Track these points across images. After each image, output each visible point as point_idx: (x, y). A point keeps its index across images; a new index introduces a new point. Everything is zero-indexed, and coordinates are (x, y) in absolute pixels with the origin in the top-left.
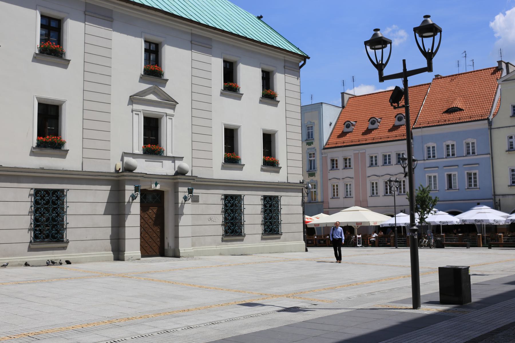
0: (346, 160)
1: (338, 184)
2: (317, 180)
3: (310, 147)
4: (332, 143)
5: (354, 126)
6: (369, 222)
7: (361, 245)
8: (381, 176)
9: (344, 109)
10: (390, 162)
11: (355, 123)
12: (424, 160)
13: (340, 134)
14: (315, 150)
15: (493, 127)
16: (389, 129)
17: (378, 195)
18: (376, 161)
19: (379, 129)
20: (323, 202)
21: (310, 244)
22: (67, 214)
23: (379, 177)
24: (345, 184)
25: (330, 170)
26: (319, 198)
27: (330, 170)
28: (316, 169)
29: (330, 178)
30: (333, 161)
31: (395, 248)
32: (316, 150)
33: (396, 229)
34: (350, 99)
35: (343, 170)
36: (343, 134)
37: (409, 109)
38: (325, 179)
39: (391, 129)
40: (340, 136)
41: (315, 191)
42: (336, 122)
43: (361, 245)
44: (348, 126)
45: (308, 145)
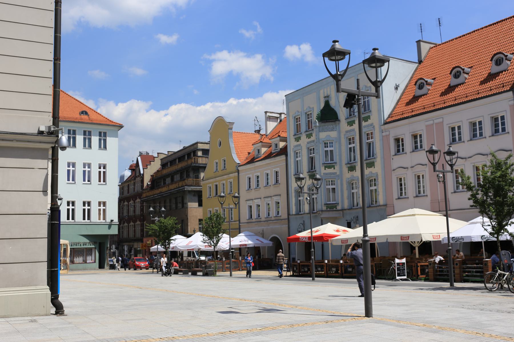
0: (415, 137)
2: (377, 173)
4: (398, 114)
5: (431, 85)
6: (420, 234)
7: (405, 277)
8: (469, 158)
9: (420, 64)
10: (504, 130)
11: (433, 81)
13: (410, 100)
14: (373, 127)
16: (482, 81)
18: (460, 134)
19: (466, 83)
20: (386, 205)
23: (486, 156)
24: (415, 175)
25: (393, 156)
26: (381, 200)
27: (393, 156)
28: (375, 156)
29: (394, 168)
30: (397, 140)
32: (374, 127)
33: (231, 253)
34: (431, 50)
35: (412, 153)
36: (415, 99)
38: (388, 170)
39: (484, 80)
40: (409, 103)
41: (376, 190)
42: (408, 83)
43: (405, 277)
44: (422, 86)
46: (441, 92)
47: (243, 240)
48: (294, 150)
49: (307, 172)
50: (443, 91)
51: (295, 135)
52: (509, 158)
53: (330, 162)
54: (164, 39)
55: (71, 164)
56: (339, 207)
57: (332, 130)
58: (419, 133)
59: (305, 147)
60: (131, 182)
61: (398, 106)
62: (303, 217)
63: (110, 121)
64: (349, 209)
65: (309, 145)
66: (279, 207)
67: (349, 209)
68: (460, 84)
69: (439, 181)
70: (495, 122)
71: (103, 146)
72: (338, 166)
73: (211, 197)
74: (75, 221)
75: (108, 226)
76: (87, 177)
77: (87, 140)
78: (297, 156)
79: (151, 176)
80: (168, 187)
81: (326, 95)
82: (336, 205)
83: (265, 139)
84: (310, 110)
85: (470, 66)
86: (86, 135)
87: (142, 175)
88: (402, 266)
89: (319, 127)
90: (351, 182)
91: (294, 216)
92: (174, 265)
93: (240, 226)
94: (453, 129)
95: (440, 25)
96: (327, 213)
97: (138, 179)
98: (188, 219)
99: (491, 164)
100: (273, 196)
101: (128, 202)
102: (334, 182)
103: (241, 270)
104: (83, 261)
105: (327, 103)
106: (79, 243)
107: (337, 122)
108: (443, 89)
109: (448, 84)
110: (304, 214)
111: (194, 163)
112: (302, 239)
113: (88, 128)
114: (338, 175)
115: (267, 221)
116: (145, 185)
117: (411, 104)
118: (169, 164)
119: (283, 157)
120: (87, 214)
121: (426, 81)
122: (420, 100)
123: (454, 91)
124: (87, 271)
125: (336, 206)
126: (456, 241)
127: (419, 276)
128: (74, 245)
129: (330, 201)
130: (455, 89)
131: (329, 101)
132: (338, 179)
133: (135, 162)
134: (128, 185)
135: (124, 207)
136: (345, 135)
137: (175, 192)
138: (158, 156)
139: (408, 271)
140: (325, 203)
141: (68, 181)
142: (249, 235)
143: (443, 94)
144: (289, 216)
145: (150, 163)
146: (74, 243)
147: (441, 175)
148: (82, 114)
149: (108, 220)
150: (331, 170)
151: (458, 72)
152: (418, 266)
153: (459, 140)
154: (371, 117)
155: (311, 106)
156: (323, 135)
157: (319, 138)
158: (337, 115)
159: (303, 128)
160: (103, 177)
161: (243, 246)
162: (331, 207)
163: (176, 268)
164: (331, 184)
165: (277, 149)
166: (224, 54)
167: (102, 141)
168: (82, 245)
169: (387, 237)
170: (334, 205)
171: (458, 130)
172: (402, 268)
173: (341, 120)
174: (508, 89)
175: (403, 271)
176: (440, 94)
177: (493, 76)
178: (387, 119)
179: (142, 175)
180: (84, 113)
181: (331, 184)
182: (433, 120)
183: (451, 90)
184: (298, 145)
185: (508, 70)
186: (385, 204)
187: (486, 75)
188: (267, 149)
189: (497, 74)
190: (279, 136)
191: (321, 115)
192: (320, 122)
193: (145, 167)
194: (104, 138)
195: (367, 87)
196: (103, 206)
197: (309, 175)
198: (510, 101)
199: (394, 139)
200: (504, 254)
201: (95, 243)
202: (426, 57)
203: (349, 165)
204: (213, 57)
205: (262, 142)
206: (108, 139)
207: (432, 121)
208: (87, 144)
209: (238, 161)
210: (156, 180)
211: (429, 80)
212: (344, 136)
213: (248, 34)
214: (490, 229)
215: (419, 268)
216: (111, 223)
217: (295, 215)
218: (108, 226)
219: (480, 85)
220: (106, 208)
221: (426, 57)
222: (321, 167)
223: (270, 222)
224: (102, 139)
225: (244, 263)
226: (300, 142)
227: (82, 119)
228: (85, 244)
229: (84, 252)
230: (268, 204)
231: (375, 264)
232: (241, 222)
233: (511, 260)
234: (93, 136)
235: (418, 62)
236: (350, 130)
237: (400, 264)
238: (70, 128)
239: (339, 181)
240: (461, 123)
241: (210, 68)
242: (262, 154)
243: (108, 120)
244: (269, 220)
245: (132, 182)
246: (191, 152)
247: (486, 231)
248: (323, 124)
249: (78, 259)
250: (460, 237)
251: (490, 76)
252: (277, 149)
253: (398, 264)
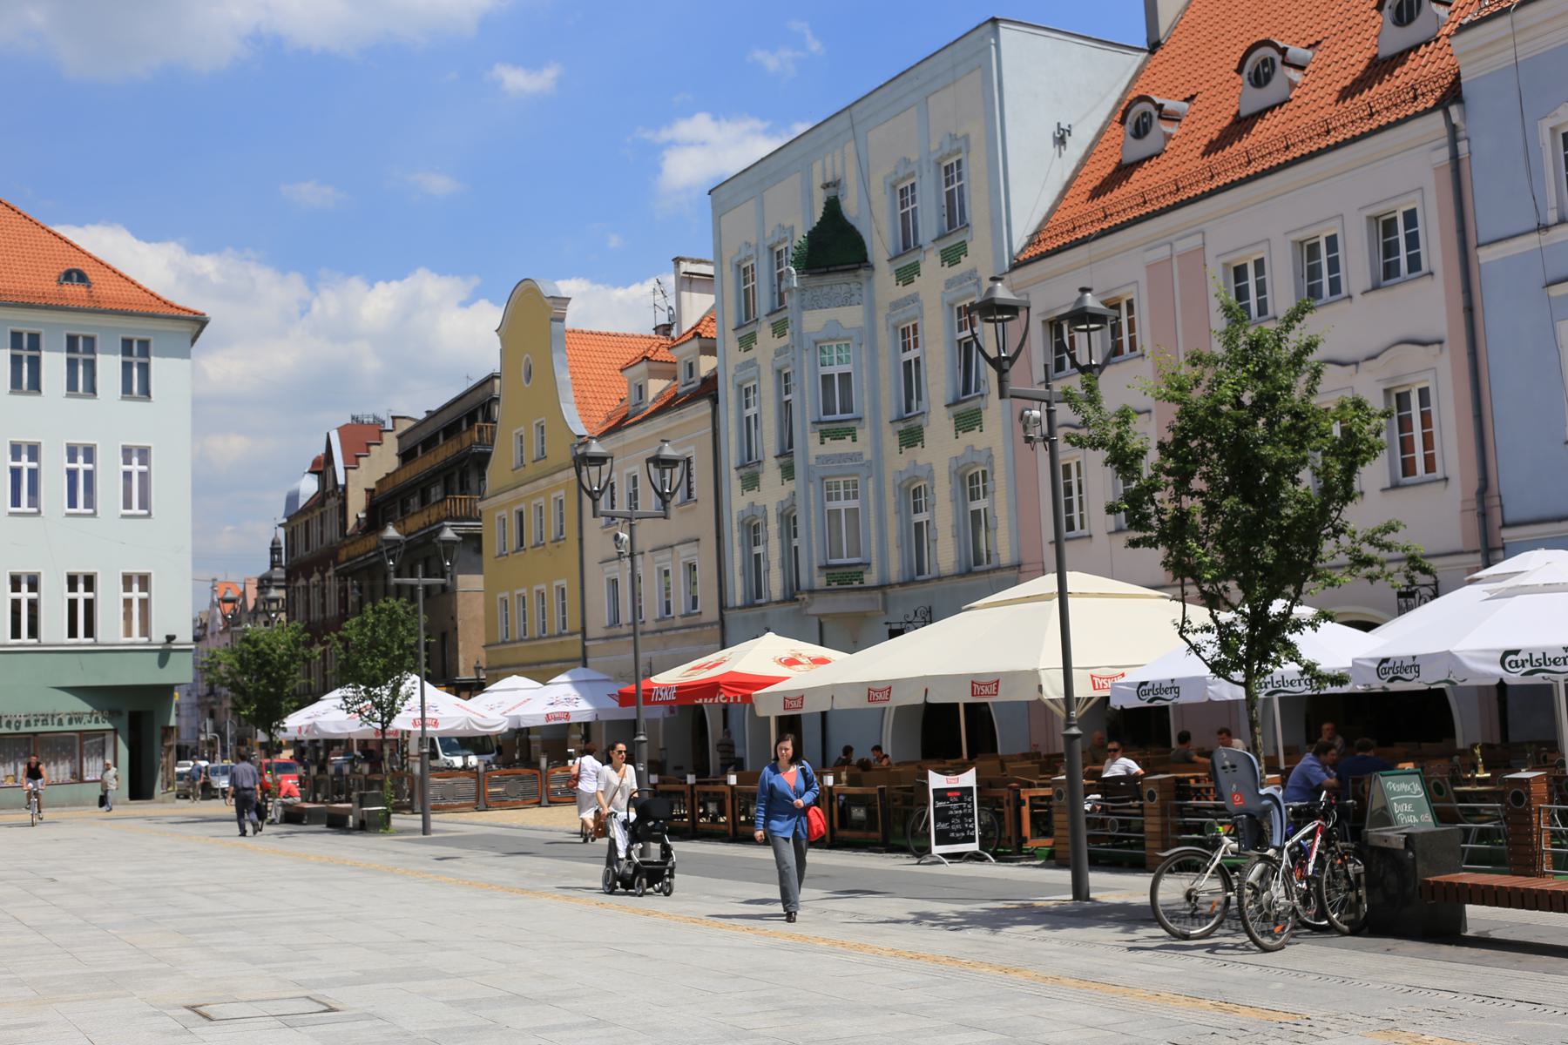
1: (1431, 385)
3: (957, 270)
6: (1035, 672)
7: (974, 847)
10: (1414, 263)
11: (1186, 105)
12: (1543, 228)
13: (1104, 181)
14: (975, 284)
16: (1345, 88)
17: (1439, 474)
19: (1291, 100)
21: (859, 825)
23: (1353, 367)
36: (1123, 171)
39: (1353, 83)
40: (1096, 193)
42: (1105, 123)
43: (974, 847)
44: (1145, 124)
45: (946, 264)
46: (1206, 141)
47: (562, 698)
48: (737, 381)
49: (776, 457)
50: (1215, 136)
51: (739, 327)
52: (1299, 321)
53: (838, 416)
54: (516, 80)
55: (25, 450)
56: (871, 578)
57: (847, 302)
58: (1125, 294)
59: (770, 368)
60: (312, 512)
61: (1064, 204)
62: (764, 616)
63: (165, 303)
64: (902, 584)
65: (781, 362)
66: (695, 584)
67: (902, 584)
68: (1271, 108)
69: (1028, 440)
70: (1384, 237)
71: (137, 385)
72: (867, 429)
73: (507, 555)
74: (40, 641)
75: (157, 655)
76: (81, 489)
77: (81, 368)
78: (747, 402)
79: (367, 490)
80: (401, 524)
81: (829, 179)
82: (860, 568)
83: (660, 350)
84: (783, 236)
85: (1312, 41)
86: (21, 348)
87: (340, 490)
88: (961, 799)
89: (802, 290)
90: (910, 485)
91: (737, 611)
92: (283, 792)
93: (584, 648)
94: (1240, 272)
96: (830, 597)
97: (332, 502)
98: (456, 629)
99: (1230, 351)
100: (678, 544)
101: (308, 577)
102: (856, 486)
103: (545, 802)
104: (72, 777)
105: (833, 209)
106: (53, 716)
107: (862, 272)
108: (1213, 132)
109: (1233, 112)
110: (770, 602)
111: (479, 443)
112: (659, 696)
113: (82, 325)
114: (867, 461)
115: (661, 631)
116: (352, 522)
117: (1105, 194)
118: (420, 449)
119: (704, 407)
120: (82, 618)
121: (1160, 107)
122: (1136, 176)
123: (1249, 133)
124: (84, 808)
125: (862, 573)
126: (1151, 701)
127: (1025, 840)
128: (37, 721)
130: (1254, 125)
131: (840, 198)
132: (868, 477)
133: (322, 450)
134: (307, 522)
135: (297, 596)
136: (888, 317)
137: (420, 541)
138: (394, 426)
139: (986, 819)
141: (70, 507)
142: (587, 681)
143: (1213, 147)
144: (725, 613)
145: (368, 451)
146: (35, 715)
147: (1036, 413)
148: (66, 279)
149: (158, 636)
150: (844, 446)
151: (1265, 62)
152: (1022, 803)
153: (1259, 315)
154: (969, 246)
155: (787, 223)
156: (814, 321)
157: (800, 333)
158: (864, 248)
159: (763, 303)
160: (138, 495)
161: (555, 719)
162: (844, 577)
163: (289, 800)
165: (692, 380)
166: (700, 125)
167: (135, 371)
168: (65, 721)
169: (926, 682)
170: (853, 570)
171: (1256, 276)
172: (961, 808)
173: (876, 266)
174: (1431, 104)
175: (962, 822)
176: (1202, 148)
177: (1384, 67)
178: (1022, 250)
179: (340, 490)
180: (75, 276)
182: (1171, 244)
183: (1239, 132)
184: (748, 362)
185: (1437, 40)
186: (1015, 561)
187: (1362, 67)
188: (667, 382)
189: (1400, 58)
190: (697, 335)
191: (809, 248)
192: (803, 273)
193: (352, 463)
194: (143, 360)
195: (956, 139)
196: (140, 591)
197: (781, 466)
198: (1435, 149)
199: (1044, 322)
200: (1227, 763)
201: (112, 714)
202: (1176, 28)
203: (901, 426)
204: (665, 135)
205: (648, 358)
206: (156, 363)
207: (1168, 247)
208: (82, 381)
209: (579, 428)
210: (383, 504)
211: (1170, 105)
212: (887, 320)
213: (771, 61)
214: (1211, 645)
215: (1026, 810)
216: (168, 647)
217: (740, 608)
218: (157, 655)
219: (1337, 101)
220: (150, 595)
221: (1173, 27)
222: (809, 434)
223: (668, 633)
224: (135, 365)
225: (558, 778)
226: (756, 351)
227: (62, 297)
228: (75, 718)
229: (73, 746)
230: (667, 573)
231: (881, 790)
232: (590, 634)
233: (1262, 792)
234: (102, 353)
235: (1146, 47)
236: (905, 299)
237: (949, 794)
238: (18, 329)
239: (871, 482)
240: (1264, 246)
241: (657, 170)
242: (650, 399)
243: (158, 299)
244: (667, 627)
245: (317, 513)
246: (476, 410)
247: (1198, 654)
248: (814, 281)
249: (52, 767)
250: (1166, 681)
251: (1376, 65)
252: (692, 380)
253: (941, 794)
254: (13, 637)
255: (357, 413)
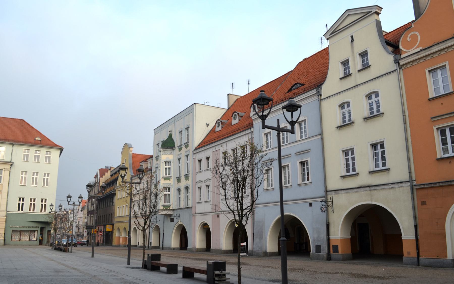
15: (323, 97)
22: (408, 184)
31: (209, 159)
37: (285, 129)
72: (172, 179)
75: (158, 245)
95: (249, 84)
105: (170, 136)
120: (32, 207)
125: (169, 206)
129: (166, 203)
140: (163, 204)
150: (168, 182)
160: (46, 182)
164: (167, 191)
181: (167, 191)
193: (101, 176)
254: (18, 210)
255: (107, 166)
